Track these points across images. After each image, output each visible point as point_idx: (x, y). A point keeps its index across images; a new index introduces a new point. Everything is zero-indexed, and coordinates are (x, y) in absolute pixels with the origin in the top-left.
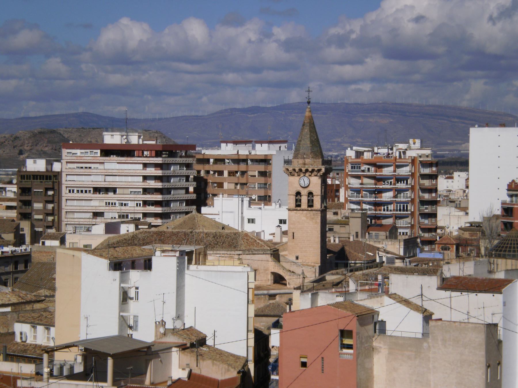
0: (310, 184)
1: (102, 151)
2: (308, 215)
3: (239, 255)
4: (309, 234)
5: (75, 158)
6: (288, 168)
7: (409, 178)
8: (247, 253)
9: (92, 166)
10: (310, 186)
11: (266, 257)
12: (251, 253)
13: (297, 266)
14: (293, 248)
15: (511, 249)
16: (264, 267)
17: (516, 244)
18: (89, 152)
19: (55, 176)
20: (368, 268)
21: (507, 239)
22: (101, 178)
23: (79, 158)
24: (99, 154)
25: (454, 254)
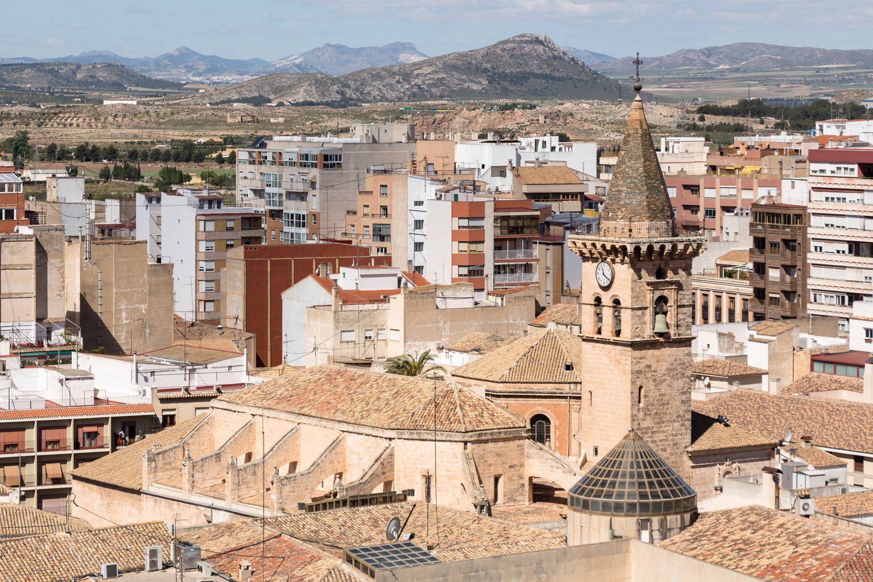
0: (615, 281)
1: (862, 166)
2: (613, 354)
3: (390, 439)
4: (613, 397)
5: (820, 180)
6: (575, 240)
7: (725, 270)
8: (407, 436)
9: (849, 196)
10: (614, 285)
11: (453, 449)
12: (415, 436)
13: (564, 472)
14: (589, 428)
15: (614, 487)
16: (448, 471)
17: (628, 476)
18: (843, 169)
19: (798, 216)
20: (388, 499)
21: (615, 461)
22: (858, 223)
23: (827, 180)
24: (856, 174)
25: (35, 505)
